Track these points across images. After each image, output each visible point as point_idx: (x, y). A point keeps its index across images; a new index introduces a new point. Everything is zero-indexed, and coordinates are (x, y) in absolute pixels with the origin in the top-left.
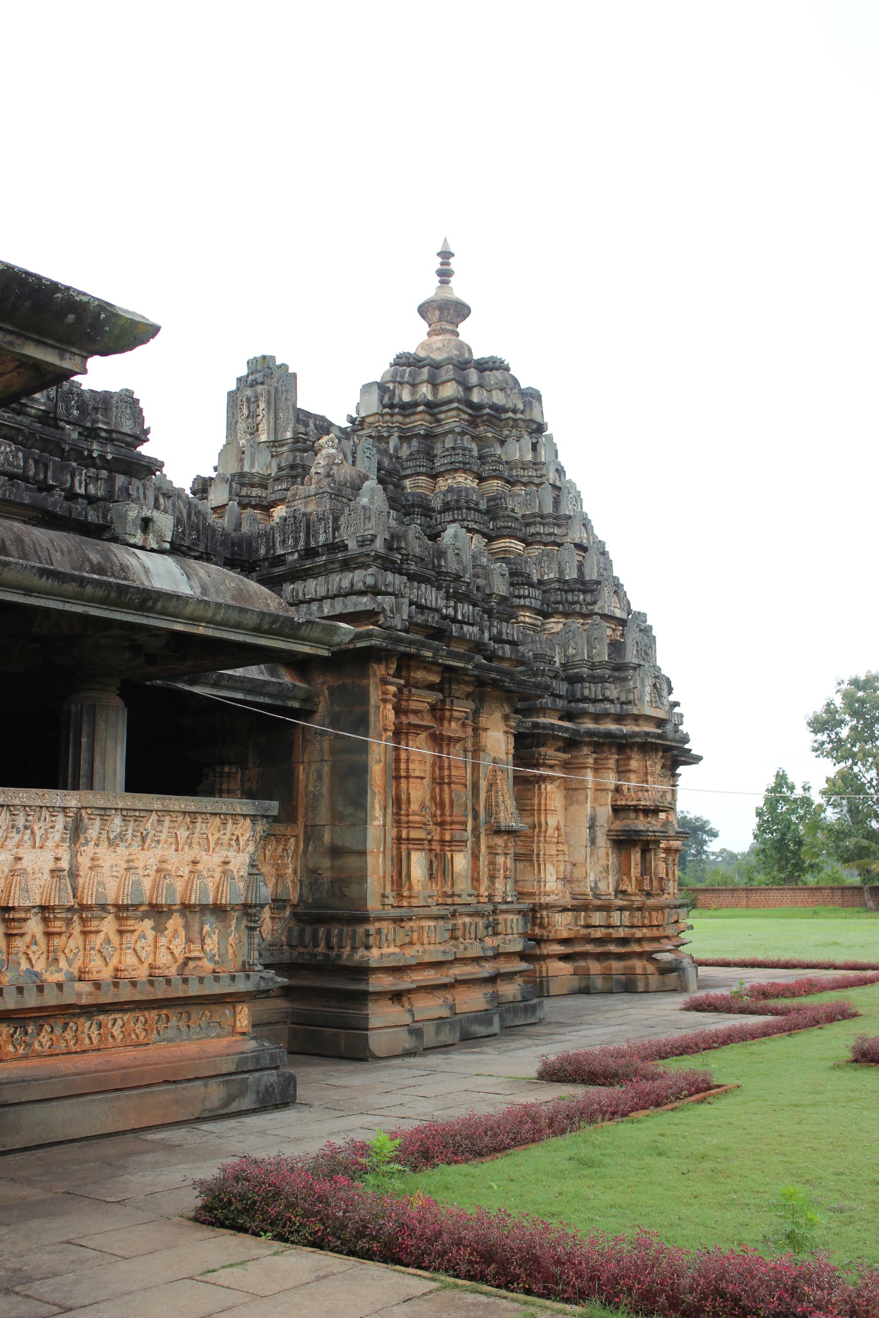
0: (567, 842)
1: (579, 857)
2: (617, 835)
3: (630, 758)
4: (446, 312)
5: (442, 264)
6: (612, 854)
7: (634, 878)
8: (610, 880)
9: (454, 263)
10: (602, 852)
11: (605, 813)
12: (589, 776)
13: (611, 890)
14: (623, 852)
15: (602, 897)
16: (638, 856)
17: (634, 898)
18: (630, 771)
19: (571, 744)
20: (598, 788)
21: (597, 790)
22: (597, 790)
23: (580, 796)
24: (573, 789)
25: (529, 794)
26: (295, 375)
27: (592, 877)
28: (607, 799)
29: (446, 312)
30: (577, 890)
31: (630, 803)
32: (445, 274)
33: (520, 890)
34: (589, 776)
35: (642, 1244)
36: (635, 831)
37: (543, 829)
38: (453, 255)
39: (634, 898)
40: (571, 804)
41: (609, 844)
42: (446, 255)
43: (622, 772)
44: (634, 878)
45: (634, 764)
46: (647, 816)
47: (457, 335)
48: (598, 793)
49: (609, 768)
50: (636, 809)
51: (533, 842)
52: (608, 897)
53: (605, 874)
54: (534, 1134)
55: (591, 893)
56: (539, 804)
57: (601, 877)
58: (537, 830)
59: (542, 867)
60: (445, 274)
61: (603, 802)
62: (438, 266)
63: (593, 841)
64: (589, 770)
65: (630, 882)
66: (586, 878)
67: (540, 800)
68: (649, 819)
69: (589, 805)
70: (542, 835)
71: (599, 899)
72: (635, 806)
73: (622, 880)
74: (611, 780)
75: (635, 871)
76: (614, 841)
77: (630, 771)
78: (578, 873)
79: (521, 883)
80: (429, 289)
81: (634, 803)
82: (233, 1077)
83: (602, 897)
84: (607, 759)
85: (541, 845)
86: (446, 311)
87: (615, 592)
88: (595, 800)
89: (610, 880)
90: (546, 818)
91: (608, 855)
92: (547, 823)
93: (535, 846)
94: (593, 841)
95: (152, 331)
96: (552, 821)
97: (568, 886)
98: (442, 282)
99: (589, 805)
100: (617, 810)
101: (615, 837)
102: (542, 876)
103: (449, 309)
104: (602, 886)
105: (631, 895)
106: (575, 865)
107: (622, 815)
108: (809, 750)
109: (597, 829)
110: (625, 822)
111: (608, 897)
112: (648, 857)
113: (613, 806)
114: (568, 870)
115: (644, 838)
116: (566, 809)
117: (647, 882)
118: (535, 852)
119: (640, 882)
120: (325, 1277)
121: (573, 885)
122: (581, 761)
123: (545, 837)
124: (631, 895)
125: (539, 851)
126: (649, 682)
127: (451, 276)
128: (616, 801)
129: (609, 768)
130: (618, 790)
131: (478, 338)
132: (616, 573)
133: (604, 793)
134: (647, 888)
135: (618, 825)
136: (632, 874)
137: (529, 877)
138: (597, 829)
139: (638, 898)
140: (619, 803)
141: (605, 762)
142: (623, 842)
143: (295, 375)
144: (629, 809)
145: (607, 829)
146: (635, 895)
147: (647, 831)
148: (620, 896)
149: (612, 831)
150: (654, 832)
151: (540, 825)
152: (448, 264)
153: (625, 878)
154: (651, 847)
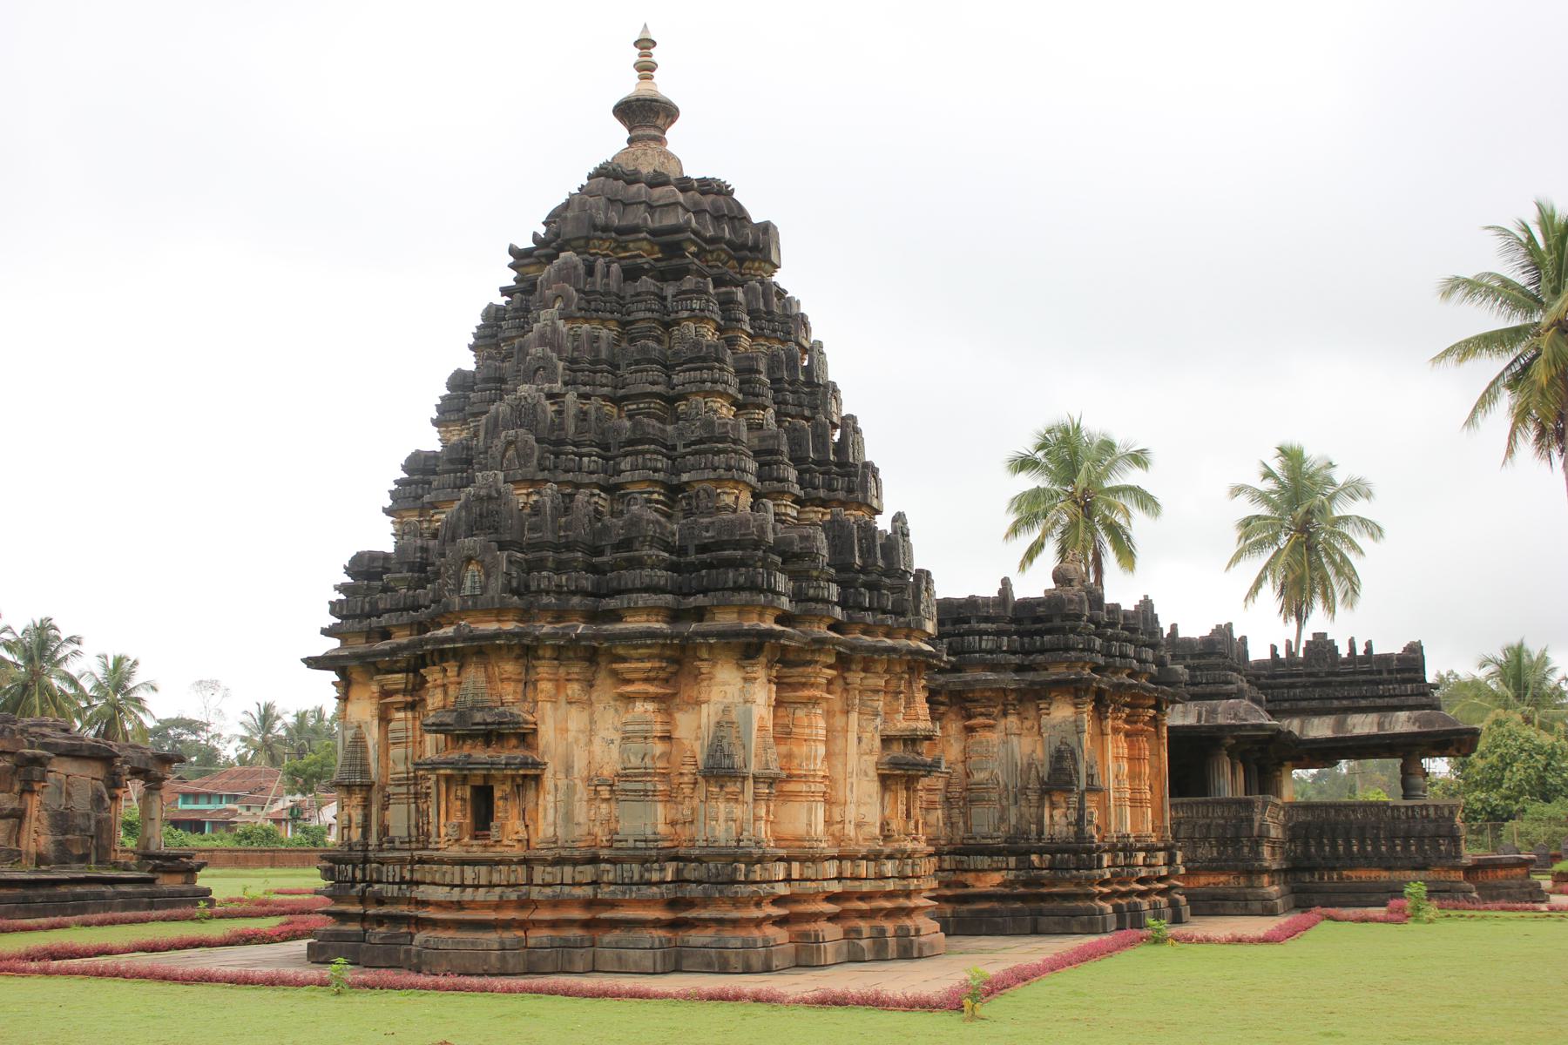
4: (645, 115)
5: (641, 56)
9: (657, 54)
19: (843, 663)
29: (645, 115)
32: (646, 69)
38: (654, 44)
42: (645, 44)
54: (1522, 750)
60: (646, 69)
80: (628, 86)
82: (79, 889)
95: (304, 660)
98: (642, 78)
120: (1329, 1034)
127: (653, 70)
131: (693, 150)
152: (650, 55)
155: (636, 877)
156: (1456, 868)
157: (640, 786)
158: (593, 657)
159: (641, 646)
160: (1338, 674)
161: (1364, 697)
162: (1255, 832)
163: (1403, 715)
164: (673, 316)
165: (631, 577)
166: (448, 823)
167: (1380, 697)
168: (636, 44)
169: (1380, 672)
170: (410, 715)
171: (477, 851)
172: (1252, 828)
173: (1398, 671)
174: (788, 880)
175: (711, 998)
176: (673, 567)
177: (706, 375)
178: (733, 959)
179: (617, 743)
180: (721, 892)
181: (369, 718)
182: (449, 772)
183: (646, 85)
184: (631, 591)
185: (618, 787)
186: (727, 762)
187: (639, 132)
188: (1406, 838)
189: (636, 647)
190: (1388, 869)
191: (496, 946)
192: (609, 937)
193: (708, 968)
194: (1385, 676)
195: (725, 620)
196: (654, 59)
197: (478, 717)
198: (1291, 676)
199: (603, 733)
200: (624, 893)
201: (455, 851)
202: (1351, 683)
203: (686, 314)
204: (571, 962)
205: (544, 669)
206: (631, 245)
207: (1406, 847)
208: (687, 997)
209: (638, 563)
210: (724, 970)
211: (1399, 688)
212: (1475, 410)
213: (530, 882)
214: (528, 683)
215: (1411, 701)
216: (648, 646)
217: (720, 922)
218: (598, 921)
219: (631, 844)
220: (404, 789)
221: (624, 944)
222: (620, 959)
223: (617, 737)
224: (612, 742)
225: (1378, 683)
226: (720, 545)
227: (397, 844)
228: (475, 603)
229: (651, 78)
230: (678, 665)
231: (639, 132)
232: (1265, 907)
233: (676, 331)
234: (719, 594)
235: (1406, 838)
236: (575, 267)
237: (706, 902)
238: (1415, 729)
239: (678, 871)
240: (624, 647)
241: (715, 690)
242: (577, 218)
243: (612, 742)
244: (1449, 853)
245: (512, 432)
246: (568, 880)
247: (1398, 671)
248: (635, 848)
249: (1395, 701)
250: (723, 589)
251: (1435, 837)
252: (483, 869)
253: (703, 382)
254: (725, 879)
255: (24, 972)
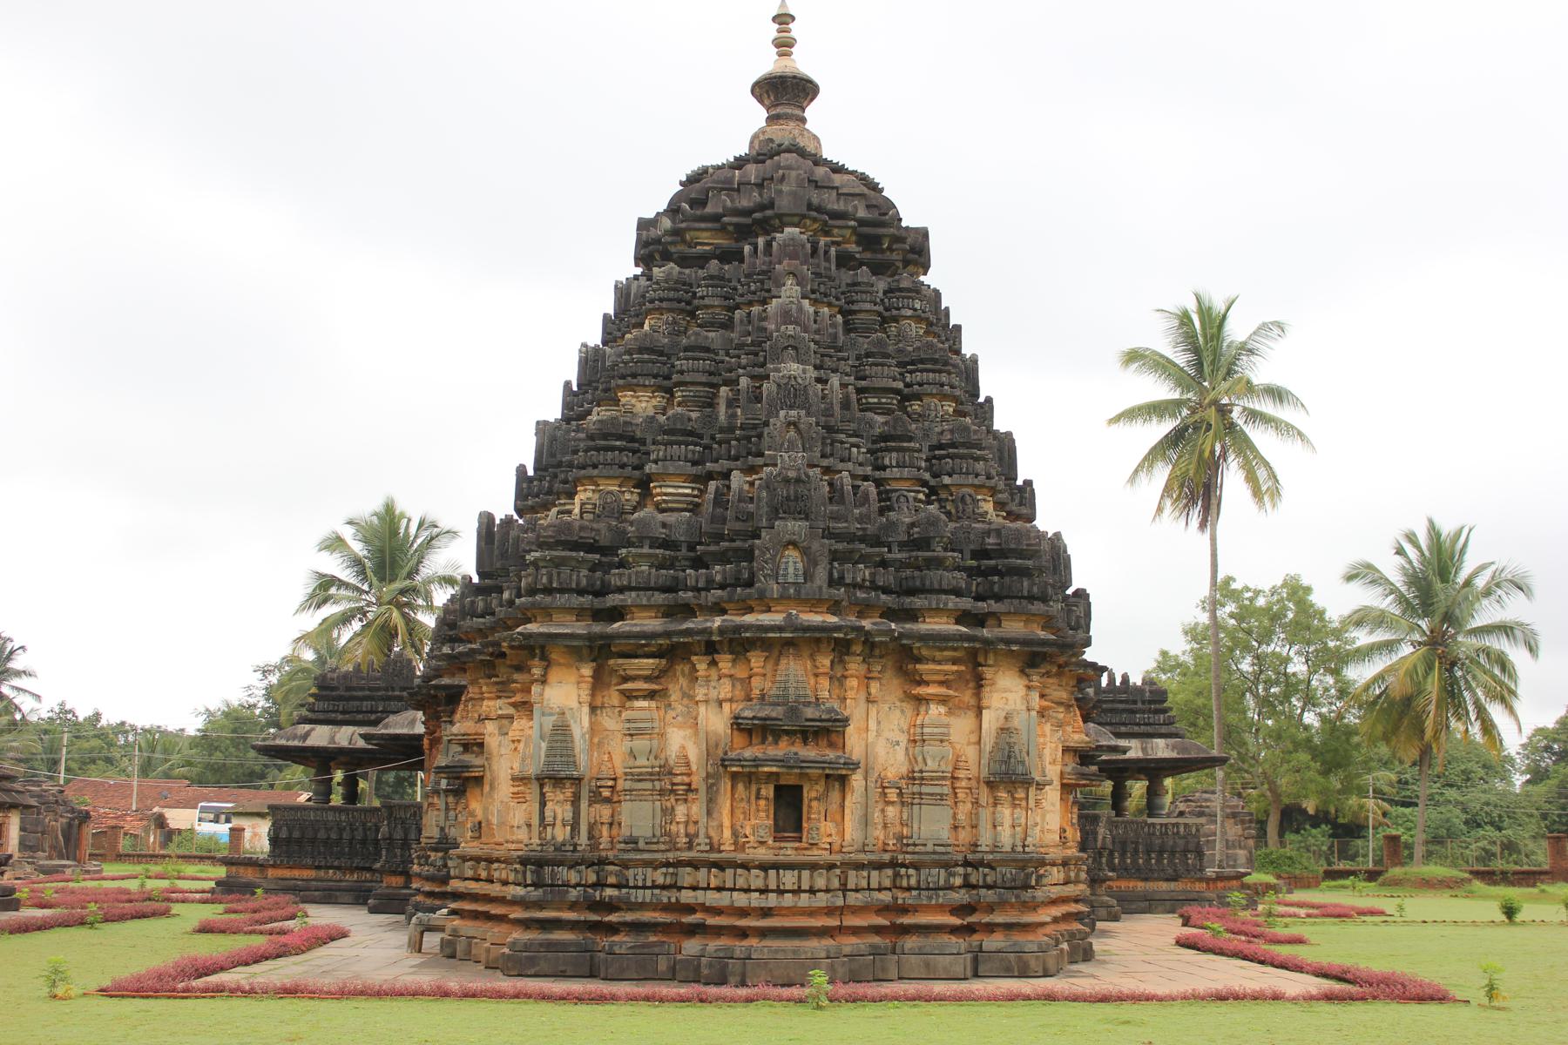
4: (786, 92)
5: (779, 31)
9: (795, 29)
26: (958, 328)
29: (786, 92)
32: (784, 45)
35: (113, 980)
38: (793, 18)
47: (804, 120)
50: (735, 865)
60: (784, 45)
62: (775, 34)
80: (767, 63)
98: (781, 55)
108: (1395, 533)
132: (193, 726)
143: (958, 328)
152: (789, 31)
155: (942, 882)
156: (1201, 880)
157: (937, 790)
158: (904, 658)
159: (946, 649)
160: (354, 689)
161: (1124, 724)
162: (1099, 844)
163: (1161, 742)
164: (895, 312)
165: (934, 577)
166: (741, 823)
167: (1138, 724)
168: (774, 19)
169: (1135, 702)
170: (653, 704)
171: (789, 852)
172: (1095, 840)
173: (1150, 702)
174: (967, 885)
175: (1038, 998)
176: (971, 572)
177: (944, 378)
178: (1033, 963)
179: (903, 744)
180: (1017, 897)
181: (575, 705)
182: (774, 769)
183: (785, 61)
184: (931, 591)
185: (914, 788)
186: (1020, 769)
187: (779, 110)
188: (1161, 852)
189: (941, 649)
190: (1146, 880)
191: (823, 955)
192: (911, 942)
193: (1008, 973)
194: (1139, 705)
195: (1014, 627)
196: (793, 34)
197: (809, 712)
198: (370, 689)
199: (886, 734)
200: (930, 898)
201: (763, 854)
202: (1111, 711)
203: (910, 313)
204: (884, 969)
205: (855, 666)
206: (835, 231)
207: (1159, 861)
208: (992, 998)
209: (938, 563)
210: (1024, 974)
211: (1153, 718)
212: (1136, 471)
213: (844, 889)
214: (839, 680)
215: (1164, 730)
216: (955, 649)
217: (1009, 927)
218: (897, 928)
219: (930, 848)
220: (648, 785)
221: (928, 950)
222: (927, 965)
223: (903, 739)
224: (898, 743)
225: (1133, 712)
226: (1002, 553)
227: (641, 845)
228: (798, 592)
229: (789, 54)
230: (974, 666)
231: (779, 110)
232: (1109, 913)
233: (893, 329)
234: (1016, 602)
235: (1173, 853)
236: (803, 246)
237: (1002, 904)
238: (1174, 755)
239: (966, 876)
240: (929, 647)
241: (995, 696)
242: (794, 194)
243: (898, 743)
244: (1194, 866)
245: (792, 413)
246: (874, 885)
247: (1150, 702)
248: (934, 853)
249: (1149, 729)
250: (1023, 597)
251: (1185, 851)
252: (806, 874)
253: (942, 385)
254: (1018, 883)
255: (187, 993)
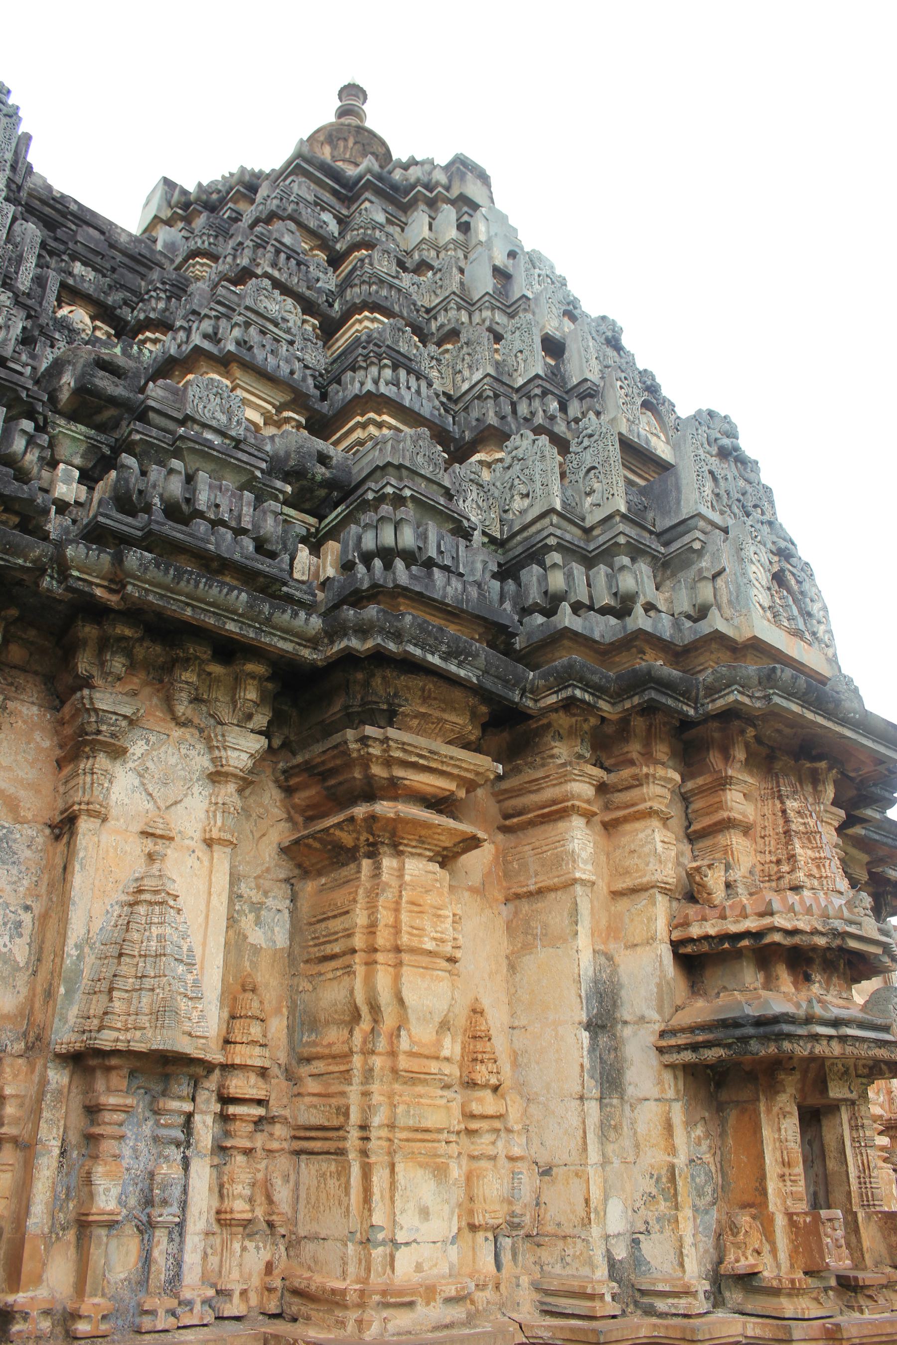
0: (520, 1087)
1: (558, 1143)
2: (694, 1047)
3: (723, 783)
6: (690, 1124)
7: (780, 1221)
8: (687, 1228)
10: (646, 1118)
11: (648, 975)
12: (579, 839)
13: (695, 1272)
14: (732, 1116)
15: (661, 1305)
16: (791, 1127)
17: (788, 1307)
18: (728, 824)
20: (620, 885)
21: (617, 895)
22: (617, 895)
23: (552, 911)
24: (530, 894)
25: (340, 897)
27: (616, 1219)
28: (652, 919)
30: (560, 1275)
31: (734, 928)
33: (302, 1278)
34: (579, 839)
36: (760, 1022)
37: (389, 1021)
39: (788, 1307)
40: (527, 948)
41: (670, 1086)
43: (702, 832)
44: (780, 1221)
45: (739, 802)
46: (808, 979)
48: (623, 904)
49: (650, 813)
51: (346, 1076)
52: (682, 1305)
53: (663, 1206)
55: (608, 1289)
56: (372, 928)
57: (651, 1217)
58: (365, 1025)
59: (380, 1179)
61: (637, 932)
63: (610, 1078)
64: (577, 822)
65: (768, 1233)
66: (586, 1223)
67: (372, 908)
68: (816, 989)
69: (584, 941)
70: (382, 1044)
71: (650, 1311)
72: (757, 935)
73: (734, 1229)
74: (659, 849)
75: (785, 1191)
76: (690, 1071)
77: (728, 824)
78: (561, 1205)
79: (309, 1248)
81: (751, 924)
83: (661, 1305)
84: (639, 782)
85: (375, 1087)
86: (341, 144)
87: (646, 405)
88: (613, 930)
89: (687, 1228)
90: (397, 978)
91: (669, 1127)
92: (401, 1001)
93: (354, 1091)
94: (610, 1078)
96: (427, 996)
97: (527, 1258)
99: (584, 941)
100: (696, 961)
101: (688, 1056)
102: (378, 1218)
103: (345, 140)
104: (657, 1253)
105: (775, 1292)
106: (546, 1172)
107: (714, 978)
109: (627, 1032)
110: (724, 999)
111: (682, 1305)
112: (829, 1138)
113: (675, 945)
114: (526, 1194)
115: (802, 1050)
116: (512, 968)
117: (834, 1234)
118: (355, 1117)
119: (807, 1236)
121: (544, 1254)
122: (549, 793)
123: (393, 1054)
124: (775, 1292)
125: (368, 1110)
126: (758, 574)
128: (686, 924)
129: (650, 813)
130: (692, 893)
133: (642, 901)
134: (839, 1262)
135: (701, 1010)
136: (774, 1203)
137: (332, 1223)
138: (627, 1032)
139: (805, 1306)
140: (695, 931)
141: (634, 794)
142: (727, 1074)
144: (738, 954)
145: (658, 1027)
146: (794, 1292)
147: (809, 1020)
148: (734, 1297)
149: (673, 1032)
150: (836, 1023)
151: (375, 1009)
153: (744, 1219)
154: (836, 1092)
